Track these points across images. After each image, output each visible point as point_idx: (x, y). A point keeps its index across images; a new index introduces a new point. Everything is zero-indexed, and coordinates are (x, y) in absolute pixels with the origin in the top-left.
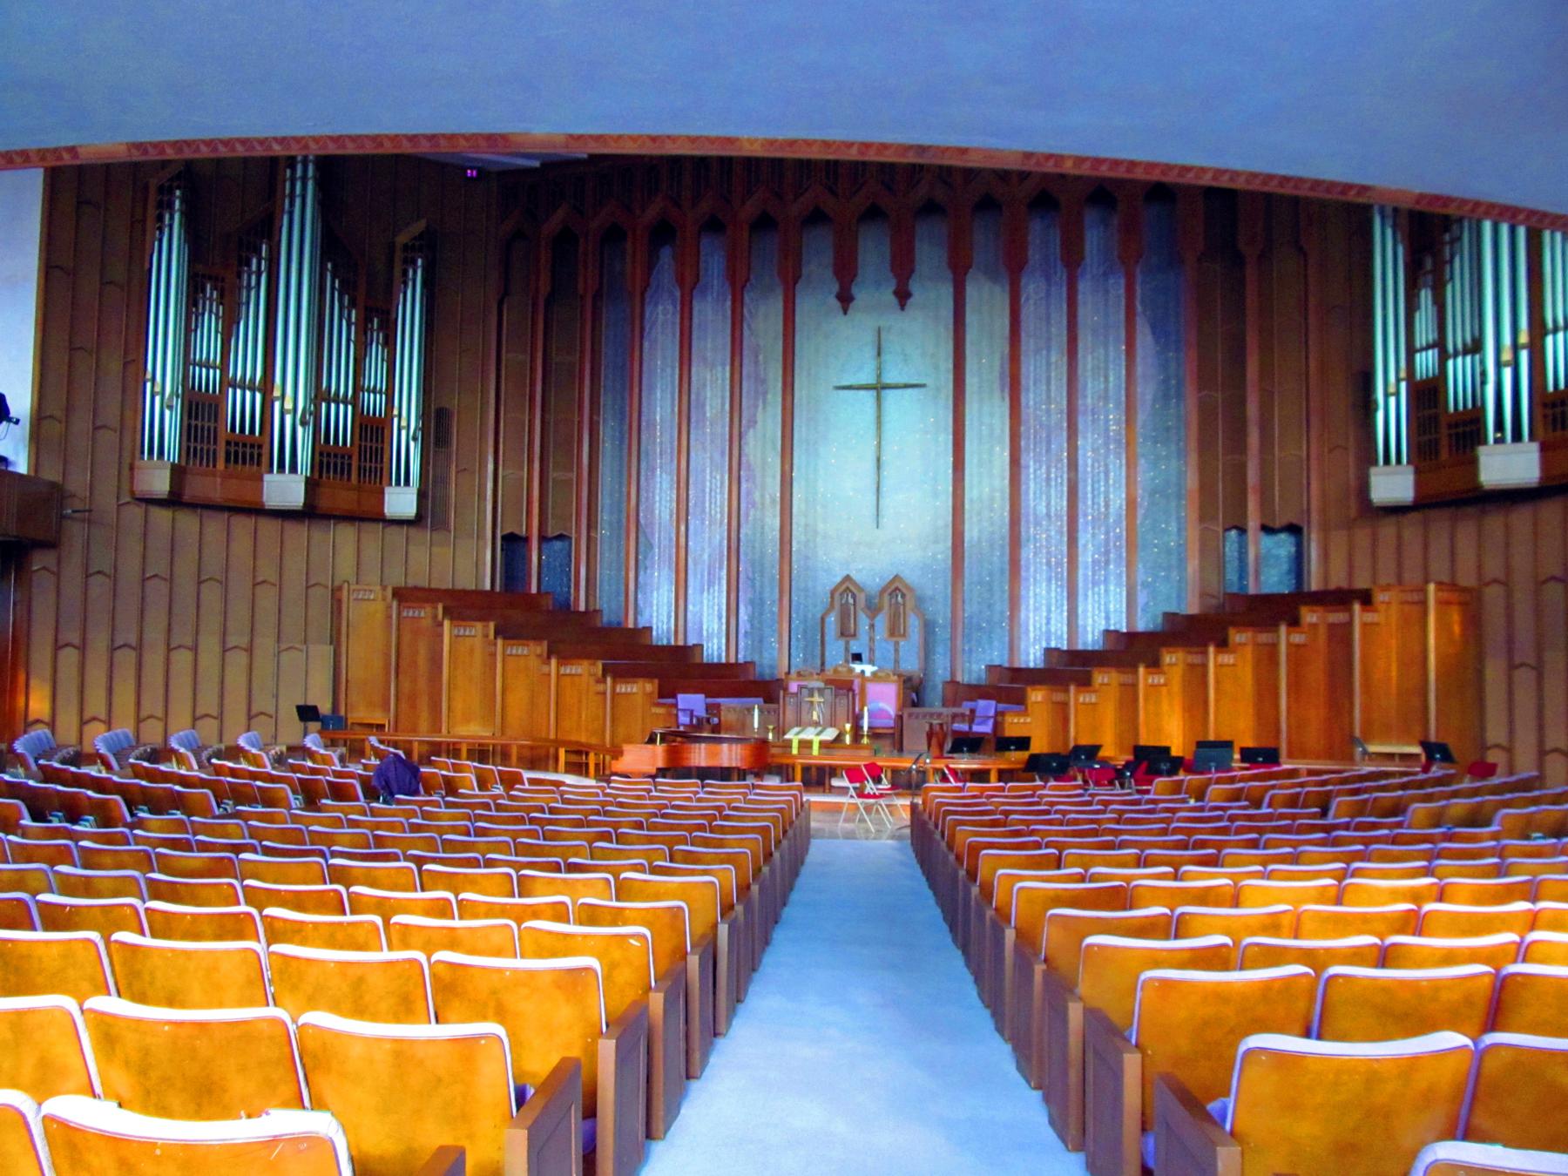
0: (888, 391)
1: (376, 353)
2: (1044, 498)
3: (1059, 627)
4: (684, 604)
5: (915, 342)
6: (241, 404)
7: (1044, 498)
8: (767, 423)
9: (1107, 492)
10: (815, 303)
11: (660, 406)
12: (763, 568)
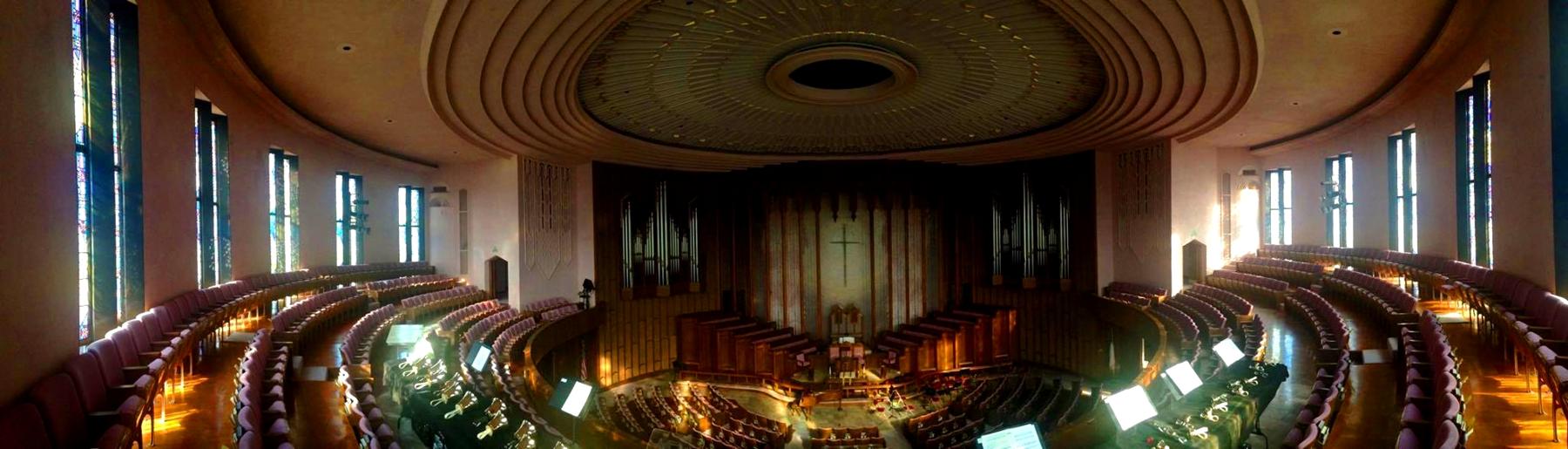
2: (898, 276)
3: (904, 315)
4: (786, 312)
5: (857, 231)
6: (649, 264)
7: (898, 276)
8: (809, 252)
9: (916, 272)
11: (775, 247)
12: (811, 298)
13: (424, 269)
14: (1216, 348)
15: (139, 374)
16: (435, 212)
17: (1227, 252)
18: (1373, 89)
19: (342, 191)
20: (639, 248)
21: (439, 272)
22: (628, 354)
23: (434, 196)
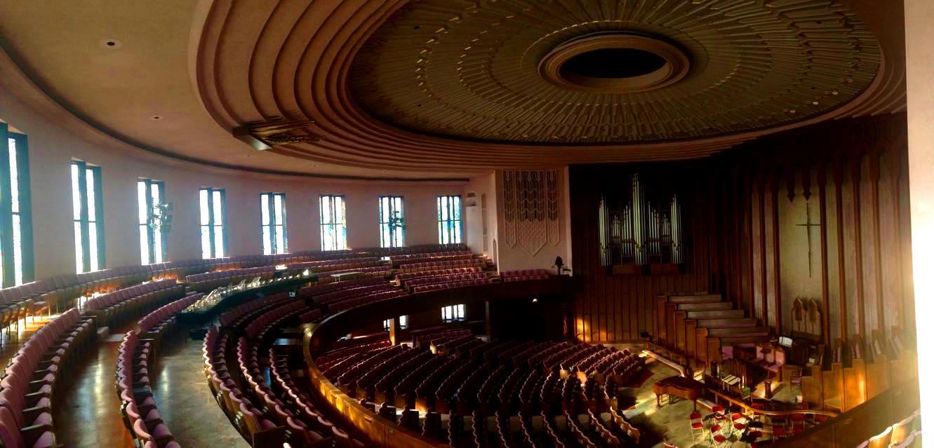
0: (814, 227)
1: (666, 225)
10: (783, 195)
13: (463, 248)
14: (732, 347)
15: (40, 385)
16: (469, 209)
17: (570, 270)
18: (303, 160)
19: (146, 198)
20: (616, 232)
21: (473, 250)
22: (611, 322)
23: (468, 199)
